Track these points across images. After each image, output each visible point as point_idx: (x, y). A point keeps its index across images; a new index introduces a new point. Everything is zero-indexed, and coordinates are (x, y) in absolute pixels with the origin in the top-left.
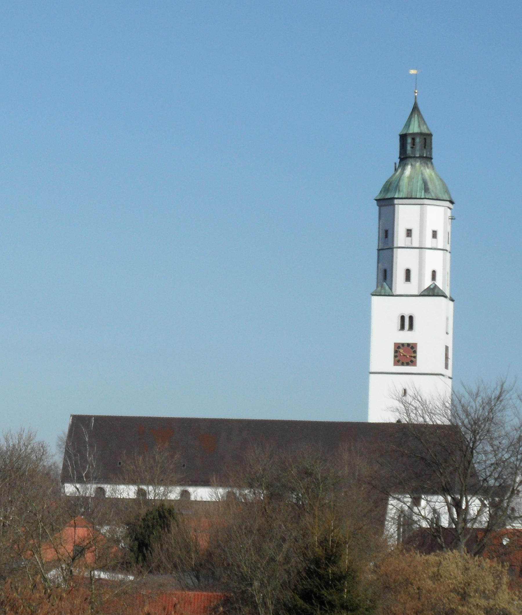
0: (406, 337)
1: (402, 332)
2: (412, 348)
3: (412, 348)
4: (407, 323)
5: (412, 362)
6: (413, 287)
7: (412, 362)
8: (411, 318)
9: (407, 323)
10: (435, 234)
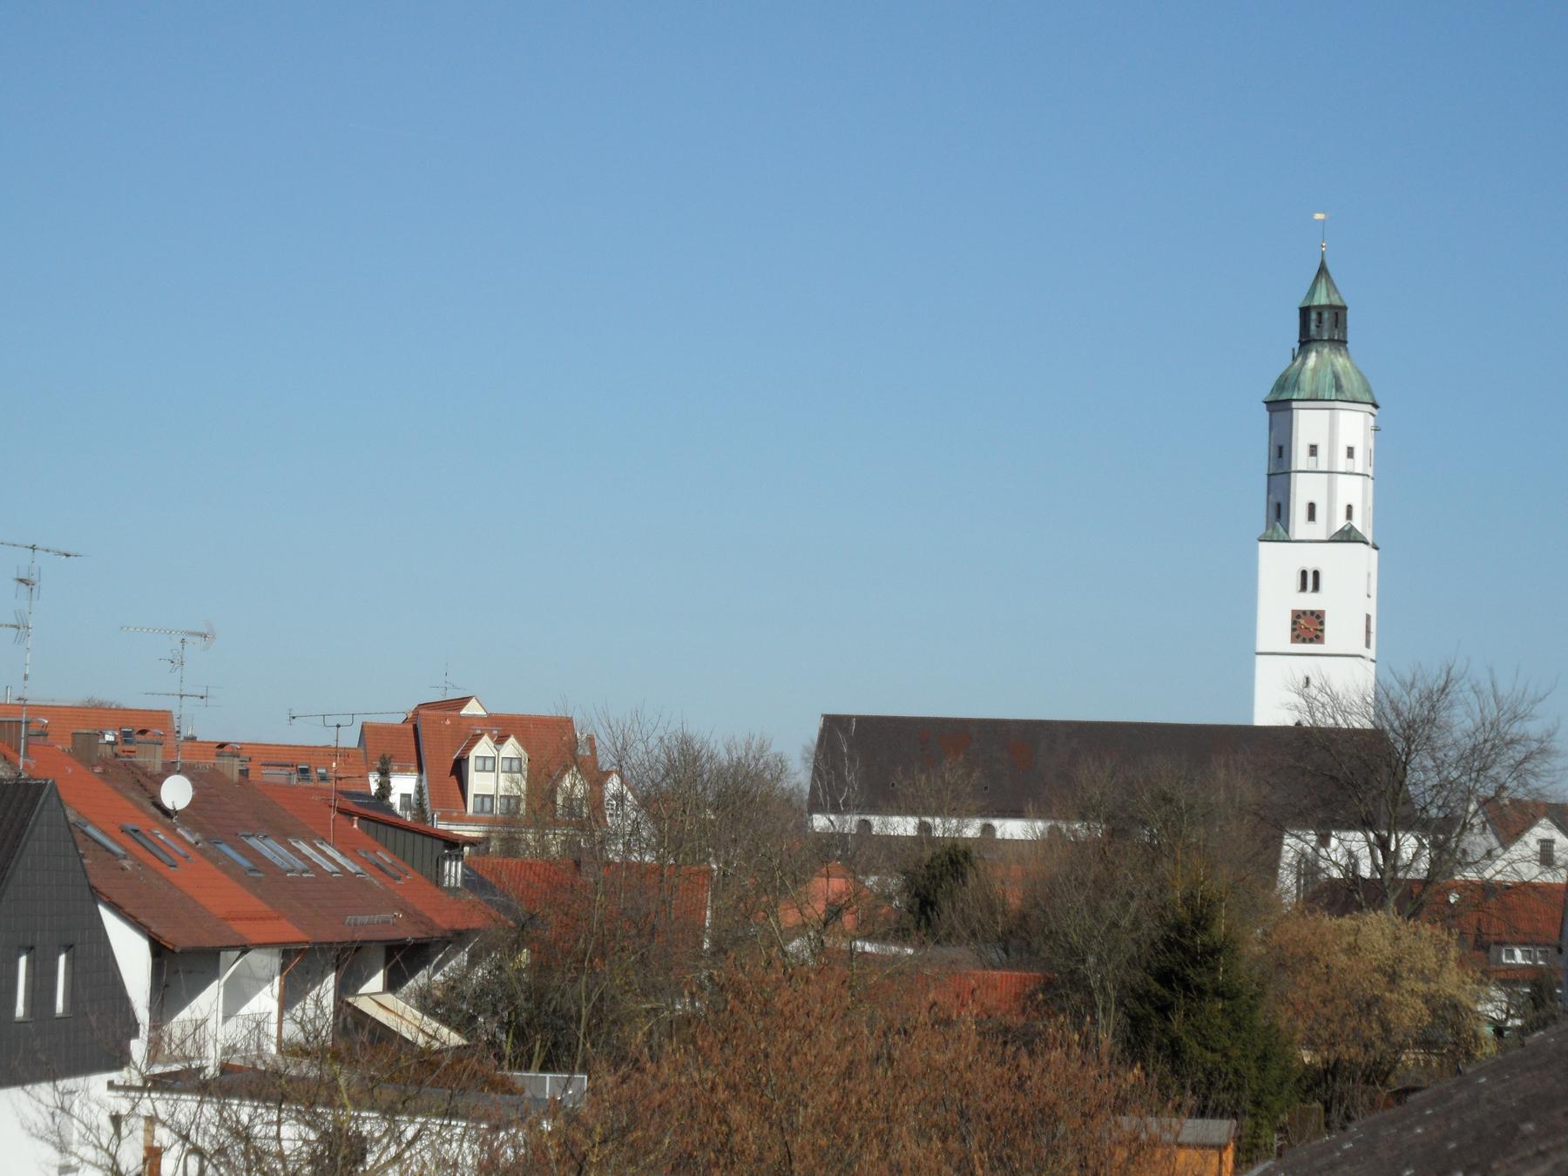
0: (1309, 602)
1: (1302, 595)
2: (1318, 617)
3: (1318, 617)
4: (1310, 580)
5: (1317, 638)
6: (1319, 530)
7: (1317, 638)
8: (1316, 574)
9: (1310, 580)
10: (1350, 452)
